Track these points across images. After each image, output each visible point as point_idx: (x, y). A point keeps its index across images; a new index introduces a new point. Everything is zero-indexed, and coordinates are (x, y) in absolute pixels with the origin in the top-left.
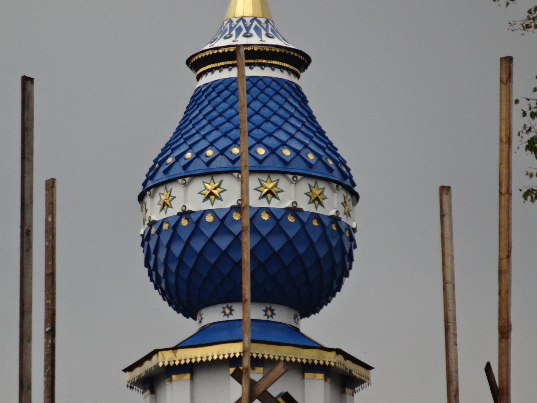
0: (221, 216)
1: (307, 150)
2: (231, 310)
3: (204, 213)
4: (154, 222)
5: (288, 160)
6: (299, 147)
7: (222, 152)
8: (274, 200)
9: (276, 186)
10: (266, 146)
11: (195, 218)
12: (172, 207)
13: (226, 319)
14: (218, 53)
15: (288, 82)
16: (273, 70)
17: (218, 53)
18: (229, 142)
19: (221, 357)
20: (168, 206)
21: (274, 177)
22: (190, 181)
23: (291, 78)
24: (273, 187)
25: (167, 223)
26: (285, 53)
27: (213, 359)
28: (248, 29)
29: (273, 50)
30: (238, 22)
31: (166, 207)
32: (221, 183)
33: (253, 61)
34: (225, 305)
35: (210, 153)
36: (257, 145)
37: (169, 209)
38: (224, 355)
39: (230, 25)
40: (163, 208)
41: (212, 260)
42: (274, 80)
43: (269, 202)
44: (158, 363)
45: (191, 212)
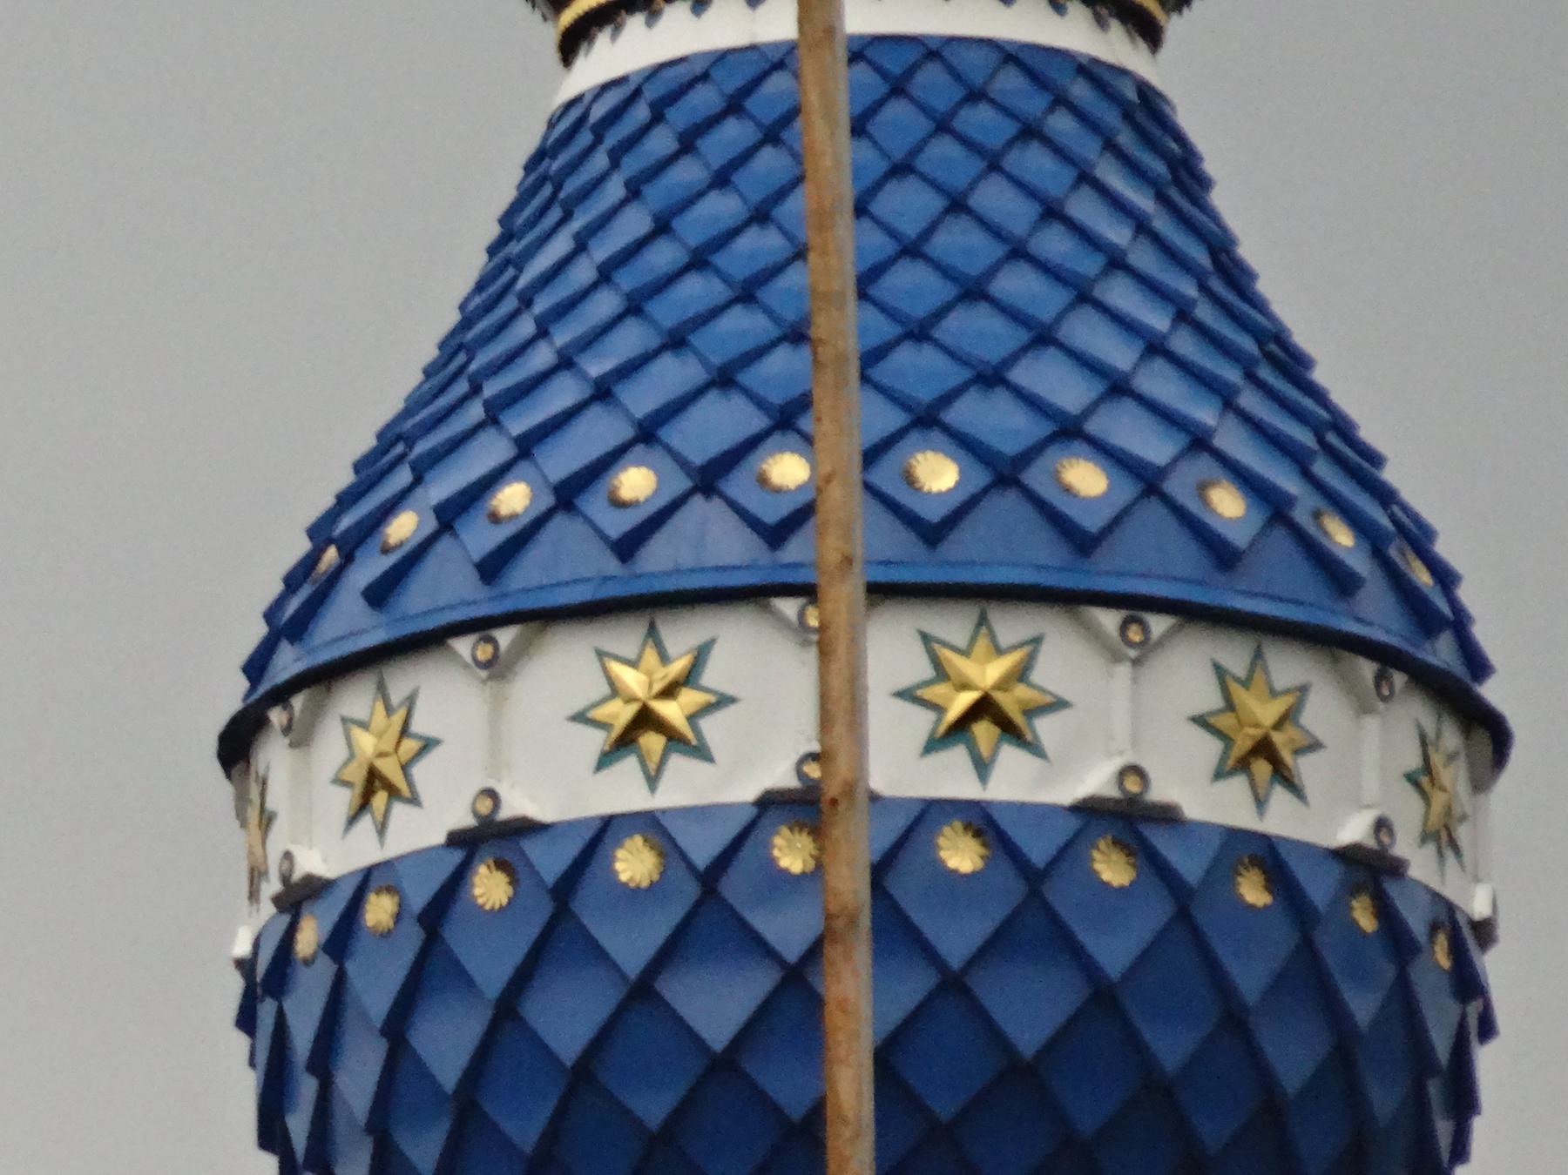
1: (1204, 465)
6: (1156, 447)
7: (708, 479)
9: (1021, 674)
10: (966, 445)
11: (551, 861)
12: (414, 800)
20: (393, 793)
22: (522, 649)
24: (1004, 684)
25: (390, 890)
32: (700, 657)
35: (636, 482)
36: (914, 436)
37: (399, 809)
40: (364, 805)
41: (653, 1108)
43: (982, 767)
45: (525, 828)
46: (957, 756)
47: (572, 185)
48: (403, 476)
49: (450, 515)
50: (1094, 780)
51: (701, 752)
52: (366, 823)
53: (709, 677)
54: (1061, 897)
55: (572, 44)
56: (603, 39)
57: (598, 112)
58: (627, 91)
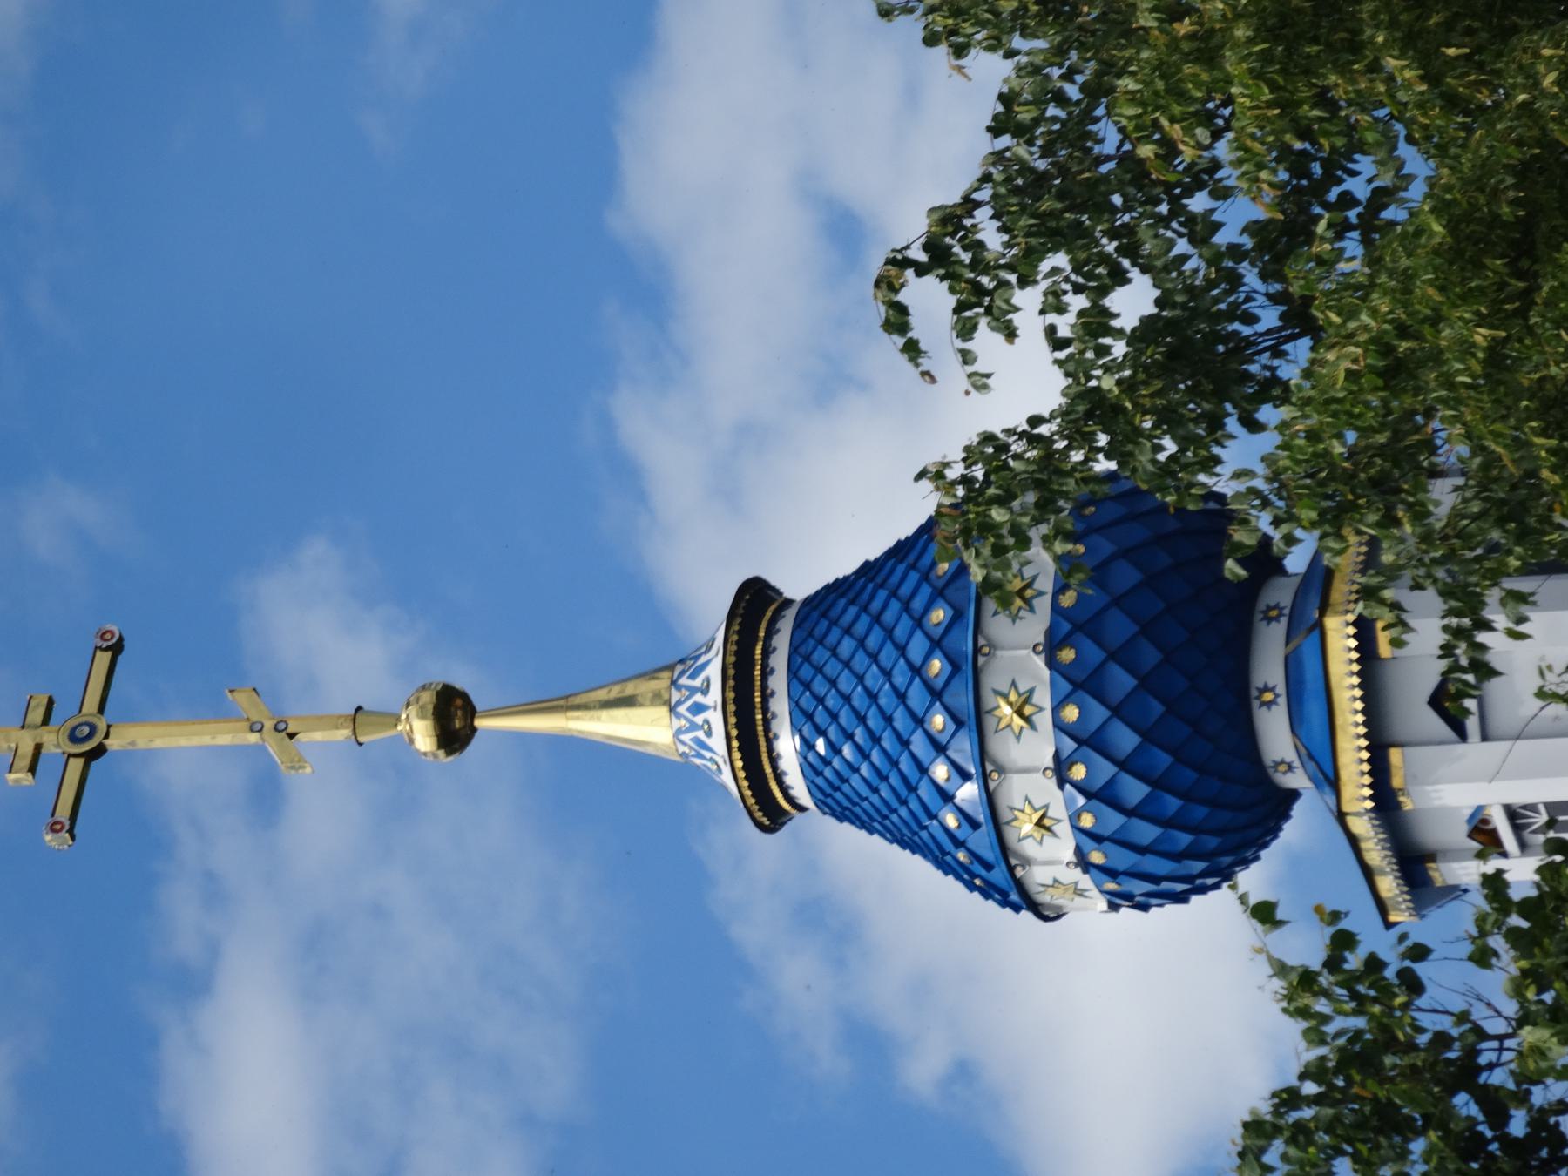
0: (1066, 687)
1: (932, 576)
2: (1266, 689)
3: (1059, 726)
4: (1079, 852)
5: (951, 612)
6: (926, 590)
7: (936, 694)
8: (1037, 585)
9: (1005, 697)
10: (928, 657)
11: (1069, 745)
12: (1047, 806)
13: (1282, 700)
14: (738, 737)
15: (797, 625)
16: (772, 671)
17: (738, 737)
18: (919, 732)
19: (1356, 667)
20: (1044, 816)
21: (989, 700)
22: (994, 762)
23: (790, 616)
24: (1011, 704)
25: (1079, 817)
26: (738, 632)
27: (1360, 686)
28: (693, 691)
29: (734, 648)
30: (679, 716)
31: (1047, 822)
32: (998, 693)
33: (757, 694)
34: (1255, 703)
35: (938, 720)
36: (926, 726)
37: (1050, 814)
38: (1360, 749)
39: (688, 730)
40: (1048, 829)
41: (1157, 708)
42: (793, 673)
43: (1040, 594)
44: (1368, 811)
45: (1057, 756)
46: (1035, 602)
47: (846, 803)
48: (948, 858)
49: (959, 844)
50: (1040, 661)
51: (1031, 691)
52: (1055, 828)
53: (1005, 690)
54: (1081, 676)
55: (802, 809)
56: (793, 793)
57: (820, 796)
58: (812, 787)
